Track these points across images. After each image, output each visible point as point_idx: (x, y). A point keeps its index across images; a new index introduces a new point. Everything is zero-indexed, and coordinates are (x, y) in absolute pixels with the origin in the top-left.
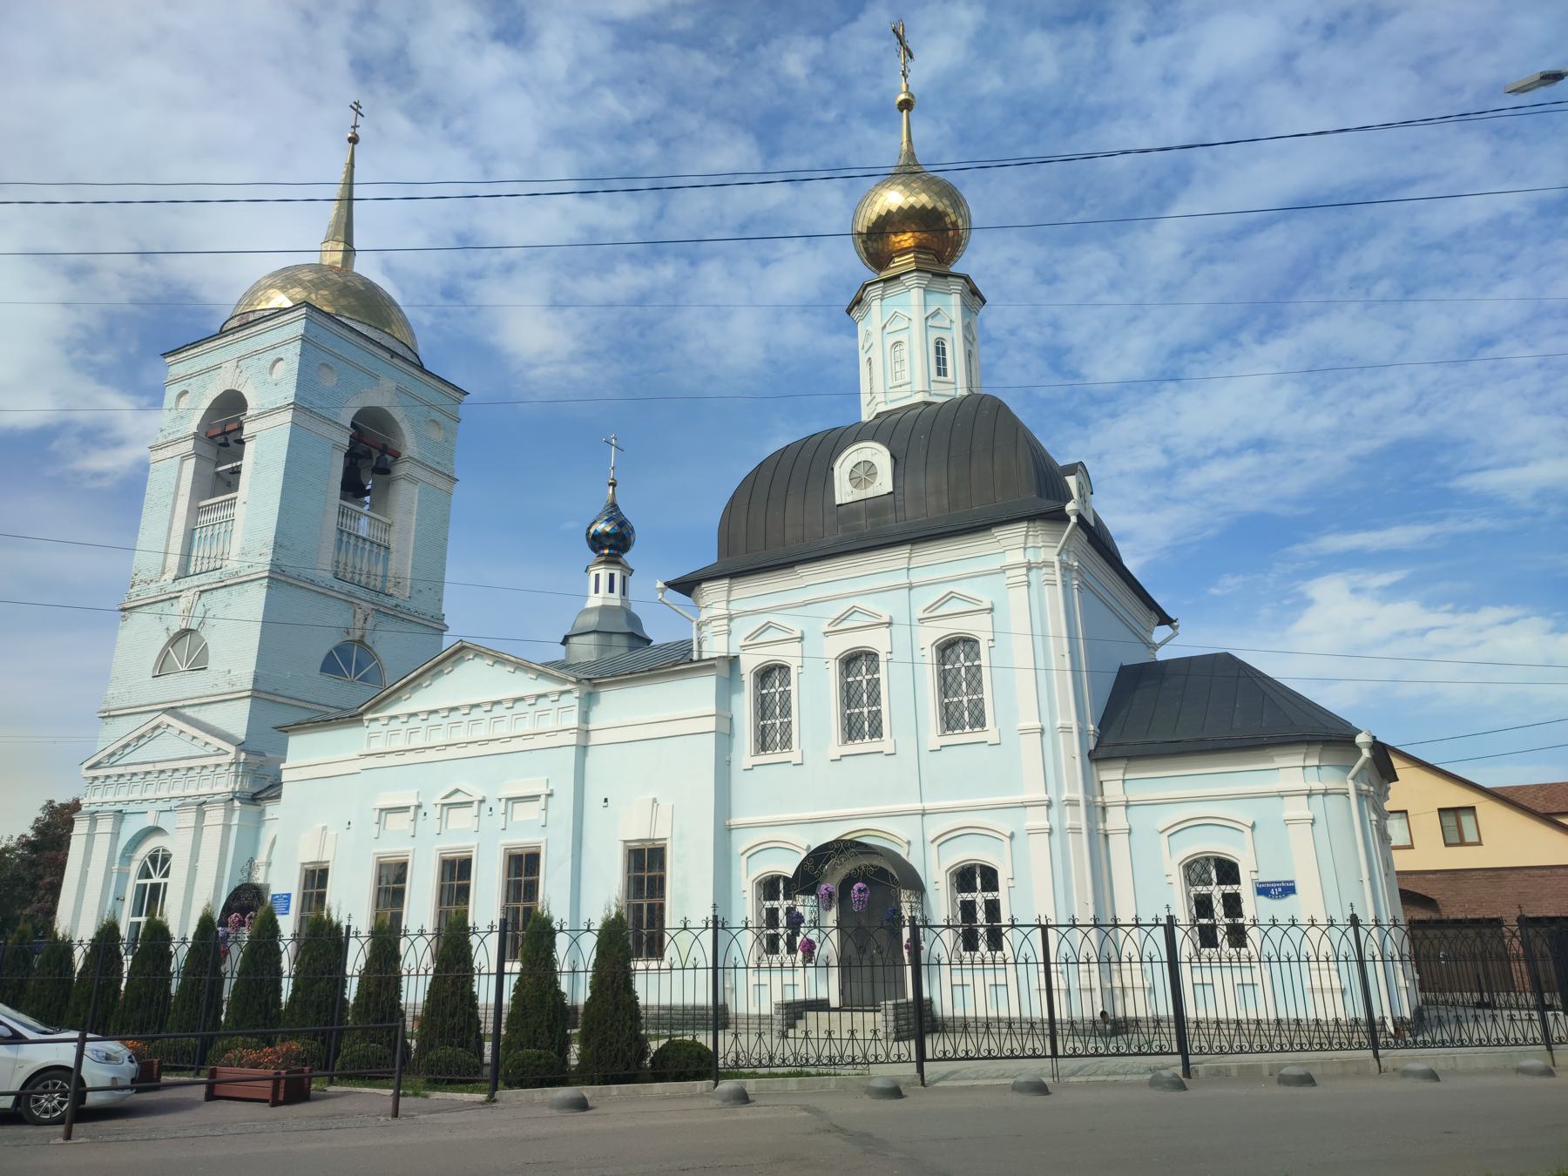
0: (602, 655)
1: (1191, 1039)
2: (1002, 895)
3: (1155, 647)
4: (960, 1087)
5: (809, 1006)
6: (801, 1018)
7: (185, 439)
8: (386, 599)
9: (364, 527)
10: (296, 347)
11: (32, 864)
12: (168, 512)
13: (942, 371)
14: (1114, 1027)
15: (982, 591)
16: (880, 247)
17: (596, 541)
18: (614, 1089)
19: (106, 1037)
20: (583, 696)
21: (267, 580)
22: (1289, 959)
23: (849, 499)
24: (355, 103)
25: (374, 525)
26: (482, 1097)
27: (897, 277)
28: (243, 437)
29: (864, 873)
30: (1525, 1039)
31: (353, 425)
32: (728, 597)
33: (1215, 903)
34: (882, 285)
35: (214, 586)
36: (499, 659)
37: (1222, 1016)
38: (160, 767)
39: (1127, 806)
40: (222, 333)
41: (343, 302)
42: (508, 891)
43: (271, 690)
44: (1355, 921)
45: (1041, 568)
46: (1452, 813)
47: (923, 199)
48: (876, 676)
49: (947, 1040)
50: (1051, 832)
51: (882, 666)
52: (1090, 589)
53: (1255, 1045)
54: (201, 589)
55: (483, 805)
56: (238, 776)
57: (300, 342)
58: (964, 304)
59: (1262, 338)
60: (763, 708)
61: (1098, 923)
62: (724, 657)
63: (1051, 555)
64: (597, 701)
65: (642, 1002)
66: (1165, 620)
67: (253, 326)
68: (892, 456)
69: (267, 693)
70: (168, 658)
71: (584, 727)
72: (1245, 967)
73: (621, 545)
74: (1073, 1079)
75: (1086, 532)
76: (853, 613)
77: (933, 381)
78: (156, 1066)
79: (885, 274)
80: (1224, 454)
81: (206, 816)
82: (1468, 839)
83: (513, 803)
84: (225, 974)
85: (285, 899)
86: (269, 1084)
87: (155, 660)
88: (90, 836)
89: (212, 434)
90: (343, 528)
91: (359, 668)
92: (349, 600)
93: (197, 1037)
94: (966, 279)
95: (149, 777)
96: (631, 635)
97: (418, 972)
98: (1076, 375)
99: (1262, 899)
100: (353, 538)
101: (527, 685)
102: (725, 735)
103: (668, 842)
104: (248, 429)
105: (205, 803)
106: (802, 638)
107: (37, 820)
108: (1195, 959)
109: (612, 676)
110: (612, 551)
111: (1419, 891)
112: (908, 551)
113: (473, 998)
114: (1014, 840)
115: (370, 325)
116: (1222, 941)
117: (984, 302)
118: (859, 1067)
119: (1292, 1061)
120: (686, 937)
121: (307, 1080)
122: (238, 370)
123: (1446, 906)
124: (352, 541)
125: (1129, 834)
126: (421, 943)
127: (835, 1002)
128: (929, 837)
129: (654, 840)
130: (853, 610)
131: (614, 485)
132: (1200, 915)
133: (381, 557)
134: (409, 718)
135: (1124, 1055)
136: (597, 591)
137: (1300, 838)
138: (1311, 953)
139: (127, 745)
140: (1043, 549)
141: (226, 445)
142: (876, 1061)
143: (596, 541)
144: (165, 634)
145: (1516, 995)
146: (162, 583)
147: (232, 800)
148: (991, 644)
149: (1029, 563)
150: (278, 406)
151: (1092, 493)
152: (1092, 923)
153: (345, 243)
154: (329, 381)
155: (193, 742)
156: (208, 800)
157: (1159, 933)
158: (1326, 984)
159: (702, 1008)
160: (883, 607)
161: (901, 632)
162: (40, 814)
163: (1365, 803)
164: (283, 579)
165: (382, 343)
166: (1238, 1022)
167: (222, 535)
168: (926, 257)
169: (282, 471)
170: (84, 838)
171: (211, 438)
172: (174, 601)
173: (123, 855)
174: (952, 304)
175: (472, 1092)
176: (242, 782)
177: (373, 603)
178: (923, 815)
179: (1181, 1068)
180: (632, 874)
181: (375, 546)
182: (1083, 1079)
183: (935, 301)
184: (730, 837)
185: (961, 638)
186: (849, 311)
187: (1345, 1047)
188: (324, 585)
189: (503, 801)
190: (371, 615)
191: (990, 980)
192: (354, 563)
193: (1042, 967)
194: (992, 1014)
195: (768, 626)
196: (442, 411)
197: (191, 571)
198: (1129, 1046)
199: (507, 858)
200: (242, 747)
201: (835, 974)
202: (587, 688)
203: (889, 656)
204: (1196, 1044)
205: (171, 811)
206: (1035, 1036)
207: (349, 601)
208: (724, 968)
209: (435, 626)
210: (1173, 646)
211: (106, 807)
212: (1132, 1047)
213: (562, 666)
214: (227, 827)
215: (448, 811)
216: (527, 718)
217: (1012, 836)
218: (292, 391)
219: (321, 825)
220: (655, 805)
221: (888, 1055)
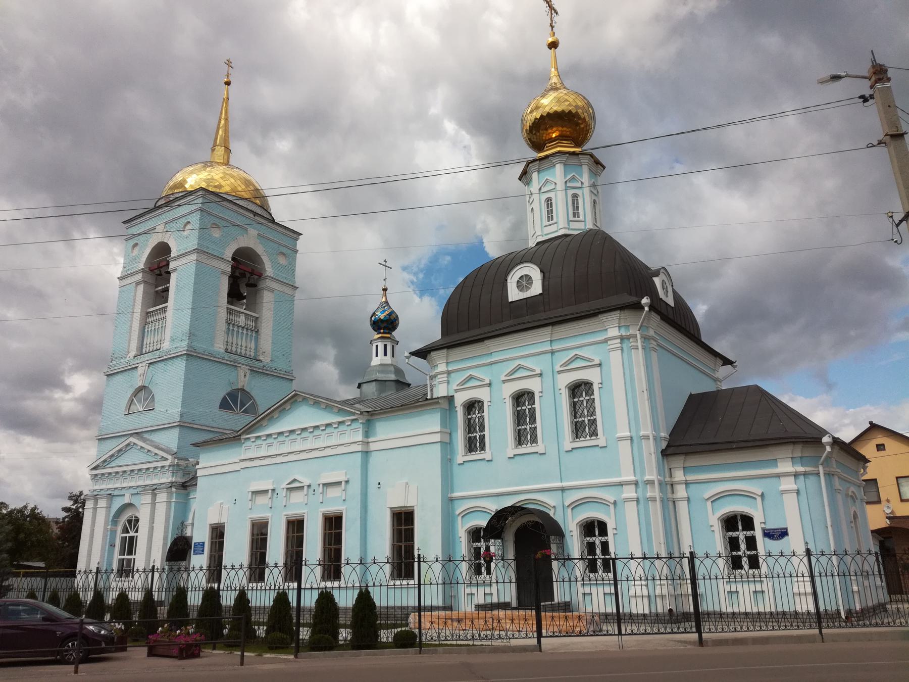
2: (610, 538)
7: (136, 273)
13: (576, 214)
20: (364, 422)
25: (250, 319)
26: (292, 657)
28: (169, 270)
31: (233, 259)
43: (190, 421)
48: (592, 397)
52: (665, 349)
54: (149, 362)
60: (470, 427)
61: (659, 556)
62: (444, 397)
65: (378, 604)
71: (366, 440)
72: (744, 581)
73: (390, 326)
75: (659, 315)
76: (519, 369)
84: (188, 589)
85: (201, 545)
88: (95, 509)
91: (242, 405)
92: (235, 364)
99: (767, 539)
100: (236, 327)
102: (447, 446)
104: (172, 265)
112: (619, 315)
117: (604, 168)
118: (505, 641)
120: (708, 562)
128: (567, 504)
133: (253, 337)
135: (649, 634)
136: (377, 355)
137: (790, 501)
141: (160, 275)
147: (171, 487)
150: (188, 250)
154: (216, 234)
155: (148, 453)
157: (685, 562)
161: (548, 378)
164: (195, 354)
165: (249, 208)
167: (160, 329)
170: (91, 510)
173: (113, 520)
177: (249, 366)
185: (583, 382)
187: (801, 628)
188: (219, 357)
191: (752, 588)
192: (237, 343)
193: (808, 579)
199: (324, 519)
200: (175, 455)
202: (366, 417)
205: (138, 494)
208: (424, 584)
209: (287, 377)
211: (102, 492)
218: (196, 242)
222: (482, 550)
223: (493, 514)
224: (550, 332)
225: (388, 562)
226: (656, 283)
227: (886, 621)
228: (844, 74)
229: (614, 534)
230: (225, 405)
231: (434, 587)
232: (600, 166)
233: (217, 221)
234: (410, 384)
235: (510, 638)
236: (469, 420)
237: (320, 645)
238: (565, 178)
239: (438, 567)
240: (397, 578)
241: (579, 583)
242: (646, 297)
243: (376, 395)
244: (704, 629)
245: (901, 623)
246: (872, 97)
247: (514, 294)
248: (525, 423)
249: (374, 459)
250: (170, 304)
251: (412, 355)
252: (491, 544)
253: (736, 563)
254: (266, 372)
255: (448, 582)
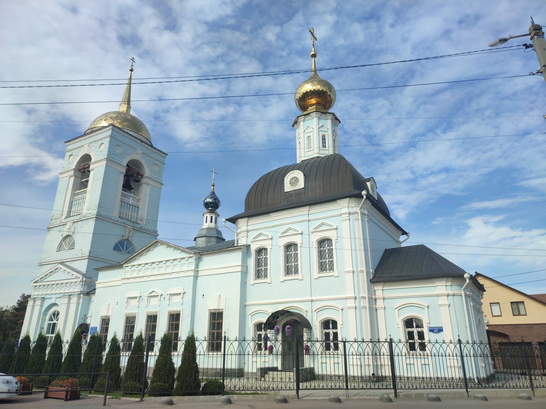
0: (207, 244)
1: (398, 384)
2: (339, 330)
3: (401, 243)
4: (312, 399)
5: (270, 369)
6: (267, 374)
7: (71, 170)
8: (137, 225)
9: (131, 201)
10: (108, 139)
11: (17, 316)
12: (64, 195)
13: (324, 146)
14: (378, 379)
15: (333, 223)
16: (304, 103)
17: (207, 205)
18: (186, 398)
19: (8, 375)
20: (196, 259)
21: (95, 218)
22: (435, 355)
23: (289, 190)
24: (132, 58)
26: (138, 399)
27: (309, 114)
29: (290, 322)
30: (524, 386)
31: (127, 165)
32: (247, 224)
33: (415, 334)
34: (304, 116)
35: (78, 220)
36: (169, 246)
37: (417, 376)
38: (57, 282)
39: (384, 299)
40: (85, 134)
41: (125, 124)
42: (169, 327)
43: (95, 256)
44: (460, 342)
45: (354, 214)
46: (515, 303)
47: (318, 87)
48: (331, 248)
49: (316, 383)
50: (356, 308)
51: (299, 248)
53: (422, 386)
54: (74, 221)
55: (162, 297)
56: (83, 286)
57: (109, 137)
58: (332, 122)
59: (444, 131)
60: (258, 263)
61: (372, 341)
62: (245, 245)
63: (357, 209)
64: (202, 261)
66: (404, 233)
67: (95, 132)
68: (304, 175)
69: (94, 257)
70: (62, 245)
71: (196, 269)
72: (331, 357)
73: (215, 206)
74: (354, 397)
76: (289, 230)
77: (321, 149)
78: (31, 386)
79: (305, 113)
80: (433, 173)
81: (71, 299)
82: (522, 313)
83: (172, 296)
85: (95, 329)
86: (65, 393)
87: (58, 245)
88: (33, 306)
89: (80, 169)
90: (123, 201)
91: (127, 249)
93: (48, 375)
94: (333, 114)
95: (53, 286)
96: (218, 238)
97: (126, 354)
98: (378, 145)
99: (431, 333)
100: (126, 204)
101: (178, 254)
102: (244, 273)
103: (224, 310)
104: (91, 167)
105: (71, 295)
106: (272, 239)
107: (19, 301)
108: (407, 355)
109: (206, 252)
110: (212, 208)
111: (502, 332)
113: (172, 364)
114: (343, 311)
115: (134, 132)
116: (417, 348)
117: (340, 122)
118: (276, 391)
119: (433, 393)
121: (79, 391)
122: (89, 147)
123: (512, 338)
124: (126, 205)
125: (384, 309)
126: (401, 345)
127: (280, 368)
128: (314, 310)
129: (219, 309)
130: (289, 229)
131: (213, 186)
132: (410, 339)
134: (138, 266)
136: (206, 222)
138: (443, 353)
139: (47, 275)
140: (355, 208)
141: (84, 172)
142: (282, 389)
143: (207, 205)
144: (61, 237)
145: (534, 371)
146: (61, 219)
147: (80, 294)
148: (336, 241)
149: (350, 212)
150: (101, 159)
151: (377, 188)
152: (370, 341)
153: (127, 104)
154: (119, 151)
156: (72, 294)
157: (386, 345)
158: (452, 365)
159: (234, 370)
160: (299, 228)
161: (306, 237)
162: (20, 299)
163: (468, 299)
164: (101, 218)
166: (423, 378)
168: (320, 107)
169: (102, 181)
171: (80, 170)
172: (65, 225)
173: (44, 313)
174: (328, 123)
175: (136, 398)
176: (84, 288)
177: (132, 226)
178: (312, 302)
179: (394, 394)
180: (212, 321)
181: (134, 207)
182: (358, 398)
183: (322, 122)
184: (246, 309)
185: (326, 239)
186: (293, 126)
187: (455, 388)
188: (115, 220)
189: (169, 295)
190: (131, 230)
192: (126, 213)
194: (333, 373)
195: (260, 234)
196: (158, 161)
197: (71, 215)
198: (382, 386)
199: (126, 318)
201: (280, 357)
202: (198, 256)
203: (301, 245)
204: (400, 385)
205: (60, 298)
206: (340, 382)
207: (124, 226)
208: (227, 355)
209: (154, 234)
210: (406, 242)
211: (39, 296)
212: (376, 386)
213: (191, 248)
214: (78, 304)
215: (172, 297)
216: (186, 265)
217: (342, 309)
219: (108, 303)
220: (220, 297)
221: (286, 387)
222: (263, 336)
223: (270, 314)
224: (308, 209)
225: (205, 340)
226: (368, 185)
227: (498, 385)
228: (509, 37)
229: (341, 328)
230: (116, 248)
231: (234, 356)
232: (337, 121)
233: (119, 143)
234: (225, 240)
235: (279, 390)
236: (259, 259)
237: (159, 393)
238: (318, 126)
239: (236, 344)
240: (211, 351)
241: (319, 356)
242: (364, 190)
243: (205, 245)
244: (398, 387)
245: (507, 386)
246: (531, 46)
247: (288, 188)
248: (291, 262)
249: (200, 281)
250: (89, 188)
251: (227, 220)
252: (268, 332)
253: (412, 347)
254: (142, 231)
255: (242, 353)
